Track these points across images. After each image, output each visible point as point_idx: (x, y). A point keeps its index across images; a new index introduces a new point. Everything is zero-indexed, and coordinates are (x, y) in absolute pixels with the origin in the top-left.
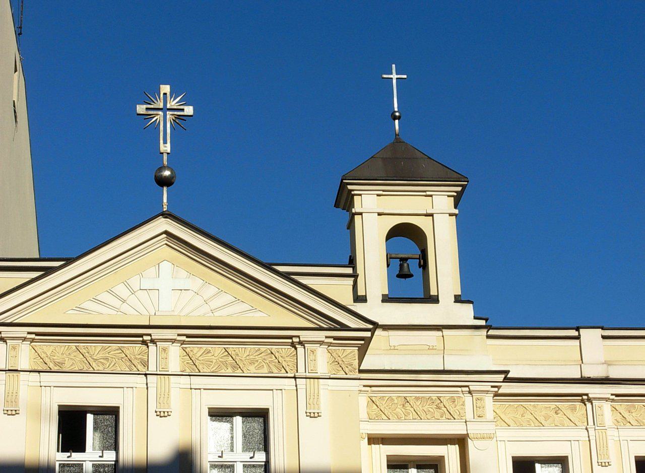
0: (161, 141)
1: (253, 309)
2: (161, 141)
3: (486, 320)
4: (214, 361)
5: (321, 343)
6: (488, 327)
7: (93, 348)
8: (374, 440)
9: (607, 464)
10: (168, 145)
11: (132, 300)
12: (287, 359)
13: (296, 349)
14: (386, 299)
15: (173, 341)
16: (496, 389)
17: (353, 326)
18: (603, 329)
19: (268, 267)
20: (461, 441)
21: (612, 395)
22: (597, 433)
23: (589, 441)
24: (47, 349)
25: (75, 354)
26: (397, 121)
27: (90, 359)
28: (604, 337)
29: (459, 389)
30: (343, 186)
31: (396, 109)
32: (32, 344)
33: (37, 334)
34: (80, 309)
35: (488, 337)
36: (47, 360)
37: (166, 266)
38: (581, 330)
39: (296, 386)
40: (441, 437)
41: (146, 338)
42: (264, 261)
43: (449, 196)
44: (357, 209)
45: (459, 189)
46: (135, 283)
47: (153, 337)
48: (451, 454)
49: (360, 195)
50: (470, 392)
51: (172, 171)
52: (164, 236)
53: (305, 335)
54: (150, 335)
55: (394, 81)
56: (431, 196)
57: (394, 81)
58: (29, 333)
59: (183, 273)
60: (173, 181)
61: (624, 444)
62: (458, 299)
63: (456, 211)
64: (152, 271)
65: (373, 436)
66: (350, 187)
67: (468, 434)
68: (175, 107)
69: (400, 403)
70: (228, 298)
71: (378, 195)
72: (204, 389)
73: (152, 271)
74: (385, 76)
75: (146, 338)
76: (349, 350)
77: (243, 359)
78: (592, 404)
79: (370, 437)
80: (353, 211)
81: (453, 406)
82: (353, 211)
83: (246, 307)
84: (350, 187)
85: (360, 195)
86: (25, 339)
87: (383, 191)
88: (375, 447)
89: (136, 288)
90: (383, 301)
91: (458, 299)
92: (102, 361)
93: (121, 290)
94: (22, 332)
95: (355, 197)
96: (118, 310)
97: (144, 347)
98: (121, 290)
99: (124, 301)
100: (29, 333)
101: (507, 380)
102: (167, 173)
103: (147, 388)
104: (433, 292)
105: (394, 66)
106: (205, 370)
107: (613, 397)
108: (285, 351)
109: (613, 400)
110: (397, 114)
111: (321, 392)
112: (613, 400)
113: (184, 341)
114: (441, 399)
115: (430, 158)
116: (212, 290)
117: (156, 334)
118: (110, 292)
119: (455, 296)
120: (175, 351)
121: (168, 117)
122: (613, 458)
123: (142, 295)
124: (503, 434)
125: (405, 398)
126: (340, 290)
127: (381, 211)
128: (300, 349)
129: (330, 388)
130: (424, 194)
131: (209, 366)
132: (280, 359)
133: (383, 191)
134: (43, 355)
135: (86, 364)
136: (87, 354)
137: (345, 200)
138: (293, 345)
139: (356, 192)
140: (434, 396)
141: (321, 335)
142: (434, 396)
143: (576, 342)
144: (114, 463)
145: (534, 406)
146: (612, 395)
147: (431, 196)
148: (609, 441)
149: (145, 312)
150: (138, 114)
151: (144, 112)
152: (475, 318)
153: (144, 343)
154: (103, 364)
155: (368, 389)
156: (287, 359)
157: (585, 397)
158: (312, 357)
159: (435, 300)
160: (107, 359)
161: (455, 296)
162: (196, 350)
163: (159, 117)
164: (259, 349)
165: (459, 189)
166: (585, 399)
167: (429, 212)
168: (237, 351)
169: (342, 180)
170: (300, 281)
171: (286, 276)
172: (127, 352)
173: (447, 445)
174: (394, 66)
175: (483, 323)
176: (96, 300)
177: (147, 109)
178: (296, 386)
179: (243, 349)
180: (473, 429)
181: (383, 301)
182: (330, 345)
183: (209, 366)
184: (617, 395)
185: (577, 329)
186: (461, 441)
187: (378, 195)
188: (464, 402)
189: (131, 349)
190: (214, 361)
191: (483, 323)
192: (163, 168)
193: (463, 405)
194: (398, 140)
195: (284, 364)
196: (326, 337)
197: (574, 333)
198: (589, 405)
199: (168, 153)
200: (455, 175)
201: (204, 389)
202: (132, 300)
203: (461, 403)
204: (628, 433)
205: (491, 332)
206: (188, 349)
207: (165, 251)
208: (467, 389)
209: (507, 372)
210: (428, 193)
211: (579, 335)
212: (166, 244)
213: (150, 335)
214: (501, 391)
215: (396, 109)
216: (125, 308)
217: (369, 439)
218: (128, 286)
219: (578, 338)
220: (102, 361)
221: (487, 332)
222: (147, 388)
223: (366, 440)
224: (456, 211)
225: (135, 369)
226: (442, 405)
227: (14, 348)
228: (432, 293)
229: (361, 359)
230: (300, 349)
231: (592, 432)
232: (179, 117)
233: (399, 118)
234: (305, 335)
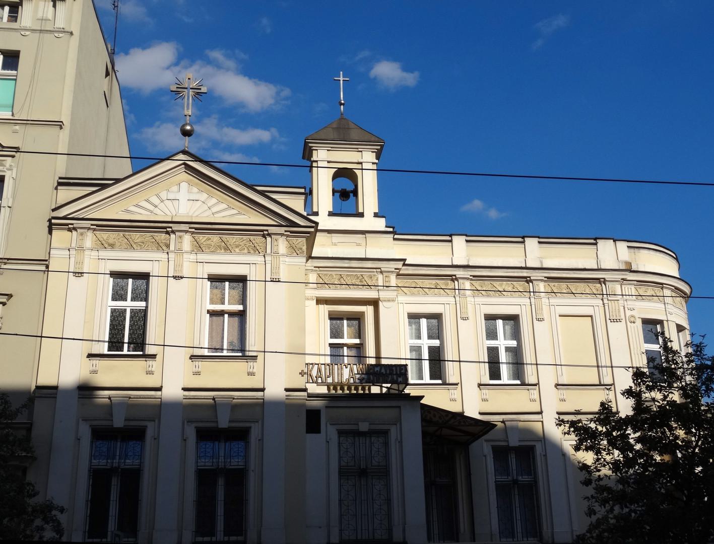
0: (186, 108)
1: (239, 213)
2: (186, 108)
3: (393, 228)
4: (213, 245)
5: (282, 235)
6: (394, 233)
7: (134, 235)
8: (320, 301)
9: (466, 319)
10: (190, 110)
11: (161, 206)
12: (260, 245)
13: (266, 238)
14: (331, 214)
15: (186, 232)
16: (398, 271)
17: (302, 224)
18: (466, 236)
19: (251, 187)
20: (375, 303)
21: (471, 276)
22: (461, 300)
23: (456, 304)
24: (104, 235)
25: (122, 239)
26: (342, 107)
27: (131, 242)
28: (467, 241)
29: (375, 270)
30: (306, 144)
31: (342, 99)
32: (94, 232)
33: (97, 226)
34: (127, 211)
35: (394, 239)
36: (103, 242)
37: (184, 186)
38: (453, 237)
39: (265, 261)
40: (363, 300)
41: (168, 229)
42: (249, 183)
43: (372, 152)
44: (314, 158)
45: (379, 147)
46: (164, 195)
47: (173, 229)
48: (369, 310)
49: (317, 150)
50: (381, 272)
51: (191, 126)
52: (183, 166)
53: (272, 230)
54: (171, 227)
55: (341, 82)
56: (361, 151)
57: (341, 82)
58: (92, 225)
59: (195, 190)
60: (192, 133)
61: (477, 306)
62: (376, 215)
63: (377, 161)
64: (175, 188)
65: (320, 299)
66: (310, 145)
67: (379, 298)
68: (195, 87)
69: (337, 278)
70: (224, 206)
71: (328, 150)
72: (206, 263)
73: (175, 188)
74: (336, 79)
75: (168, 229)
76: (300, 240)
77: (232, 244)
78: (458, 282)
79: (318, 299)
80: (312, 159)
81: (371, 280)
82: (312, 159)
83: (235, 212)
84: (310, 145)
85: (317, 150)
86: (89, 229)
87: (332, 148)
88: (321, 307)
89: (164, 198)
90: (329, 215)
91: (376, 215)
92: (140, 244)
93: (155, 200)
94: (87, 224)
95: (314, 151)
96: (151, 212)
97: (168, 236)
98: (155, 200)
99: (156, 206)
100: (92, 225)
101: (404, 265)
102: (188, 128)
103: (168, 262)
104: (361, 210)
105: (341, 72)
106: (207, 251)
107: (471, 277)
108: (259, 239)
109: (471, 280)
110: (343, 102)
111: (281, 265)
112: (471, 279)
113: (194, 232)
114: (363, 276)
115: (361, 128)
116: (214, 201)
117: (175, 227)
118: (147, 201)
119: (375, 213)
120: (187, 238)
121: (190, 93)
122: (470, 315)
123: (167, 202)
124: (402, 299)
125: (341, 275)
126: (297, 203)
127: (329, 160)
128: (269, 239)
129: (287, 263)
130: (357, 150)
131: (209, 248)
132: (256, 245)
133: (332, 148)
134: (101, 239)
135: (129, 245)
136: (130, 239)
137: (307, 153)
138: (264, 236)
139: (314, 148)
140: (359, 274)
141: (282, 230)
142: (359, 274)
143: (450, 244)
144: (144, 308)
145: (422, 282)
146: (471, 276)
147: (361, 151)
148: (468, 305)
149: (168, 213)
150: (172, 91)
151: (175, 89)
152: (386, 227)
153: (167, 233)
154: (141, 245)
155: (317, 269)
156: (260, 245)
157: (454, 277)
158: (275, 243)
159: (361, 215)
160: (143, 243)
161: (375, 213)
162: (202, 238)
163: (184, 93)
164: (242, 238)
165: (379, 147)
166: (453, 278)
167: (360, 161)
168: (228, 239)
169: (306, 140)
170: (272, 196)
171: (262, 193)
172: (156, 238)
173: (366, 305)
174: (341, 72)
175: (391, 230)
176: (137, 206)
177: (177, 88)
178: (265, 261)
179: (232, 238)
180: (383, 295)
181: (329, 215)
182: (288, 236)
183: (209, 248)
184: (474, 276)
185: (451, 236)
186: (375, 303)
187: (328, 150)
188: (378, 278)
189: (159, 237)
190: (213, 245)
191: (391, 230)
192: (186, 124)
193: (377, 280)
194: (342, 118)
195: (258, 248)
196: (286, 231)
197: (448, 238)
198: (456, 282)
199: (190, 116)
200: (377, 139)
201: (206, 263)
202: (161, 206)
203: (376, 279)
204: (480, 300)
205: (396, 236)
206: (197, 237)
207: (184, 176)
208: (379, 270)
209: (404, 260)
210: (359, 150)
211: (452, 239)
212: (185, 171)
213: (171, 227)
214: (401, 272)
215: (342, 99)
216: (156, 211)
217: (317, 300)
218: (158, 196)
219: (451, 241)
220: (140, 244)
221: (394, 236)
222: (168, 262)
223: (315, 301)
224: (377, 161)
225: (161, 249)
226: (363, 280)
227: (82, 234)
228: (360, 211)
229: (50, 20)
230: (269, 239)
231: (458, 299)
232: (198, 93)
233: (343, 104)
234: (272, 230)
